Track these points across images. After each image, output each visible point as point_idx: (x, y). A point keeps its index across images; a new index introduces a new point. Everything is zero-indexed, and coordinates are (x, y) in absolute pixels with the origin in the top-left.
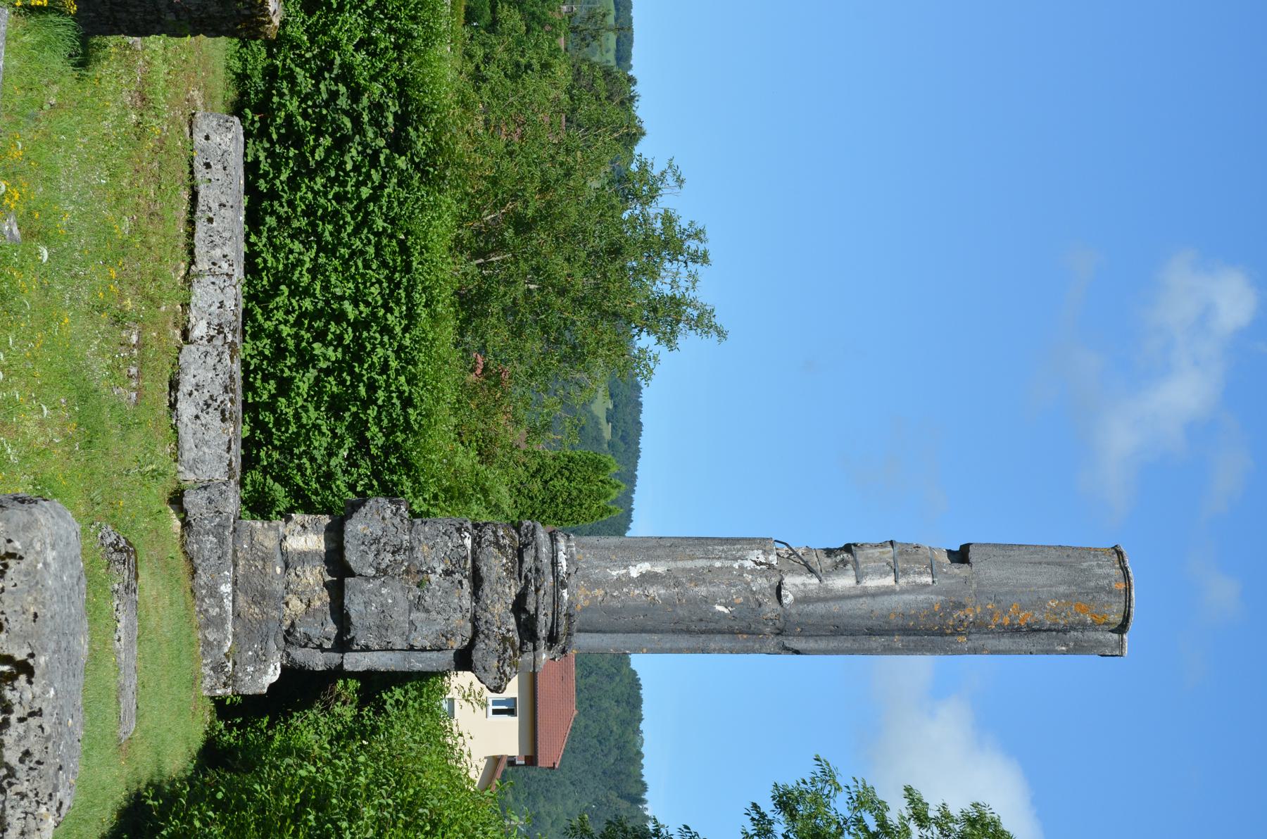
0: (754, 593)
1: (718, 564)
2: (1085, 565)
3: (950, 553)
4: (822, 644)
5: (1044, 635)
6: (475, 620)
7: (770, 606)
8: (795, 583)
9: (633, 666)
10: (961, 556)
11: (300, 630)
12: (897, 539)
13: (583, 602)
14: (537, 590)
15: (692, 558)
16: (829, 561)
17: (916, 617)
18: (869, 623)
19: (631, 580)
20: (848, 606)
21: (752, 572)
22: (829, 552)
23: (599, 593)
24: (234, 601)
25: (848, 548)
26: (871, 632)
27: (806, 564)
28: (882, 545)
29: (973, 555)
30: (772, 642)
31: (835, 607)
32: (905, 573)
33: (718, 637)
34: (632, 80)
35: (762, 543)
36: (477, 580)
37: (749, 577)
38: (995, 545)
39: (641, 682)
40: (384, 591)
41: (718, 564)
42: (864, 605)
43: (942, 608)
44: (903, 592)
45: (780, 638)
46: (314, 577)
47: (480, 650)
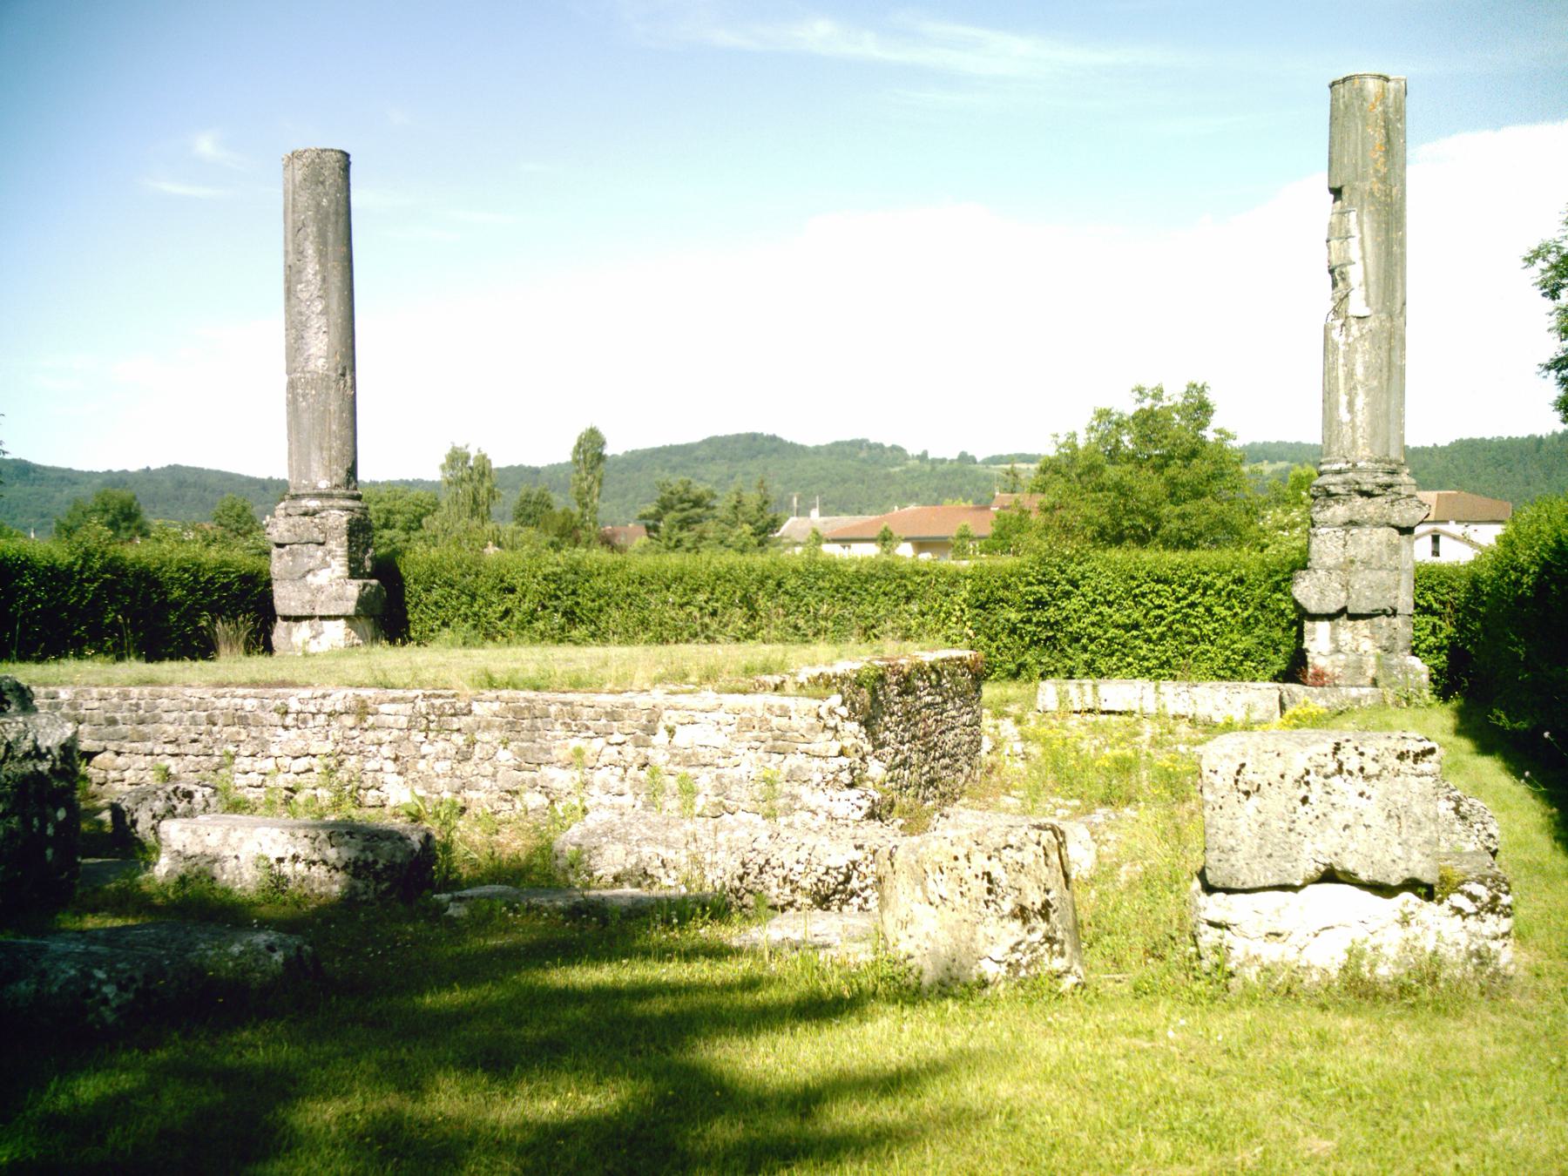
0: (1362, 335)
1: (1341, 361)
2: (1342, 107)
3: (1335, 201)
4: (1399, 287)
5: (1391, 134)
6: (1378, 525)
7: (1372, 324)
8: (1357, 305)
9: (620, 453)
10: (1337, 193)
11: (1385, 643)
12: (1326, 238)
13: (1367, 452)
14: (1358, 483)
15: (1337, 378)
16: (1340, 285)
17: (1379, 223)
18: (1383, 255)
19: (1352, 420)
20: (1371, 269)
21: (1347, 336)
22: (1335, 285)
23: (1360, 442)
24: (1363, 686)
25: (1331, 271)
26: (1389, 253)
27: (1341, 300)
28: (1329, 248)
29: (1338, 185)
30: (1398, 322)
31: (1372, 278)
32: (1348, 231)
33: (1394, 359)
34: (923, 457)
35: (1327, 330)
36: (1353, 523)
37: (1351, 340)
38: (1330, 170)
39: (970, 454)
40: (1357, 587)
41: (1341, 361)
42: (1370, 261)
43: (1373, 204)
44: (1361, 232)
45: (974, 847)
46: (1345, 630)
47: (1402, 518)
